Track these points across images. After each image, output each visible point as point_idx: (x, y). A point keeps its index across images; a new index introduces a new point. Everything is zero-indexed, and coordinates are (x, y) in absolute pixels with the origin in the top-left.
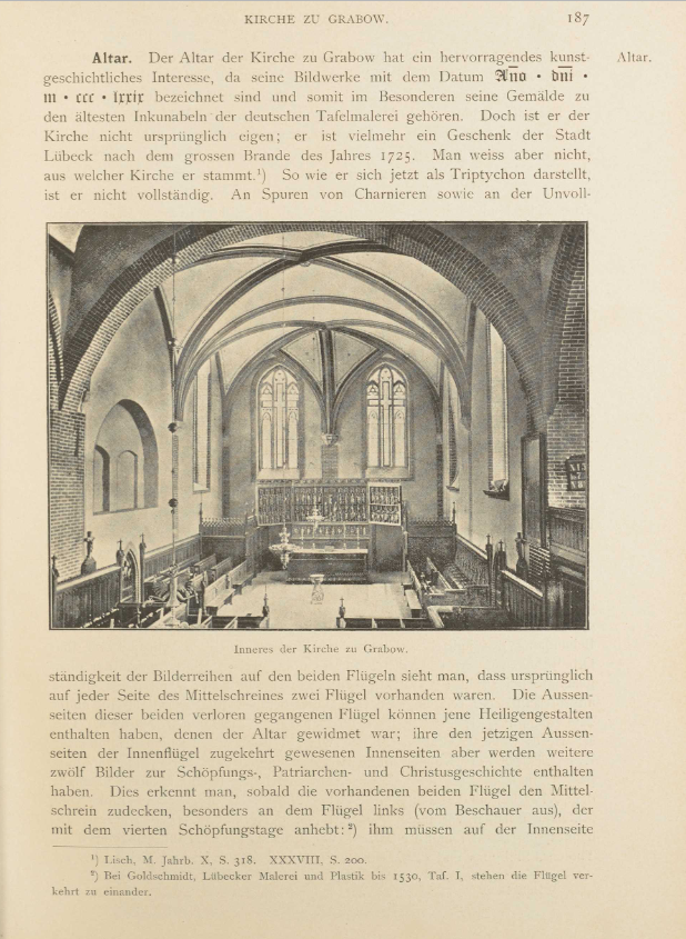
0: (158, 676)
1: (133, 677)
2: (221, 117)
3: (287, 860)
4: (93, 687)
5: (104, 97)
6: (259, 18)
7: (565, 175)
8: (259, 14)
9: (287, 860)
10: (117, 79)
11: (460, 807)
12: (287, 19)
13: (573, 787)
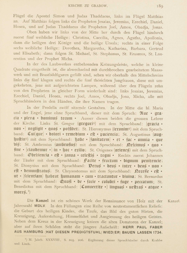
0: (84, 201)
1: (97, 201)
2: (85, 102)
3: (50, 240)
4: (54, 214)
5: (99, 161)
6: (72, 5)
7: (120, 207)
8: (72, 4)
9: (50, 240)
10: (37, 48)
11: (15, 186)
12: (80, 5)
13: (97, 32)
